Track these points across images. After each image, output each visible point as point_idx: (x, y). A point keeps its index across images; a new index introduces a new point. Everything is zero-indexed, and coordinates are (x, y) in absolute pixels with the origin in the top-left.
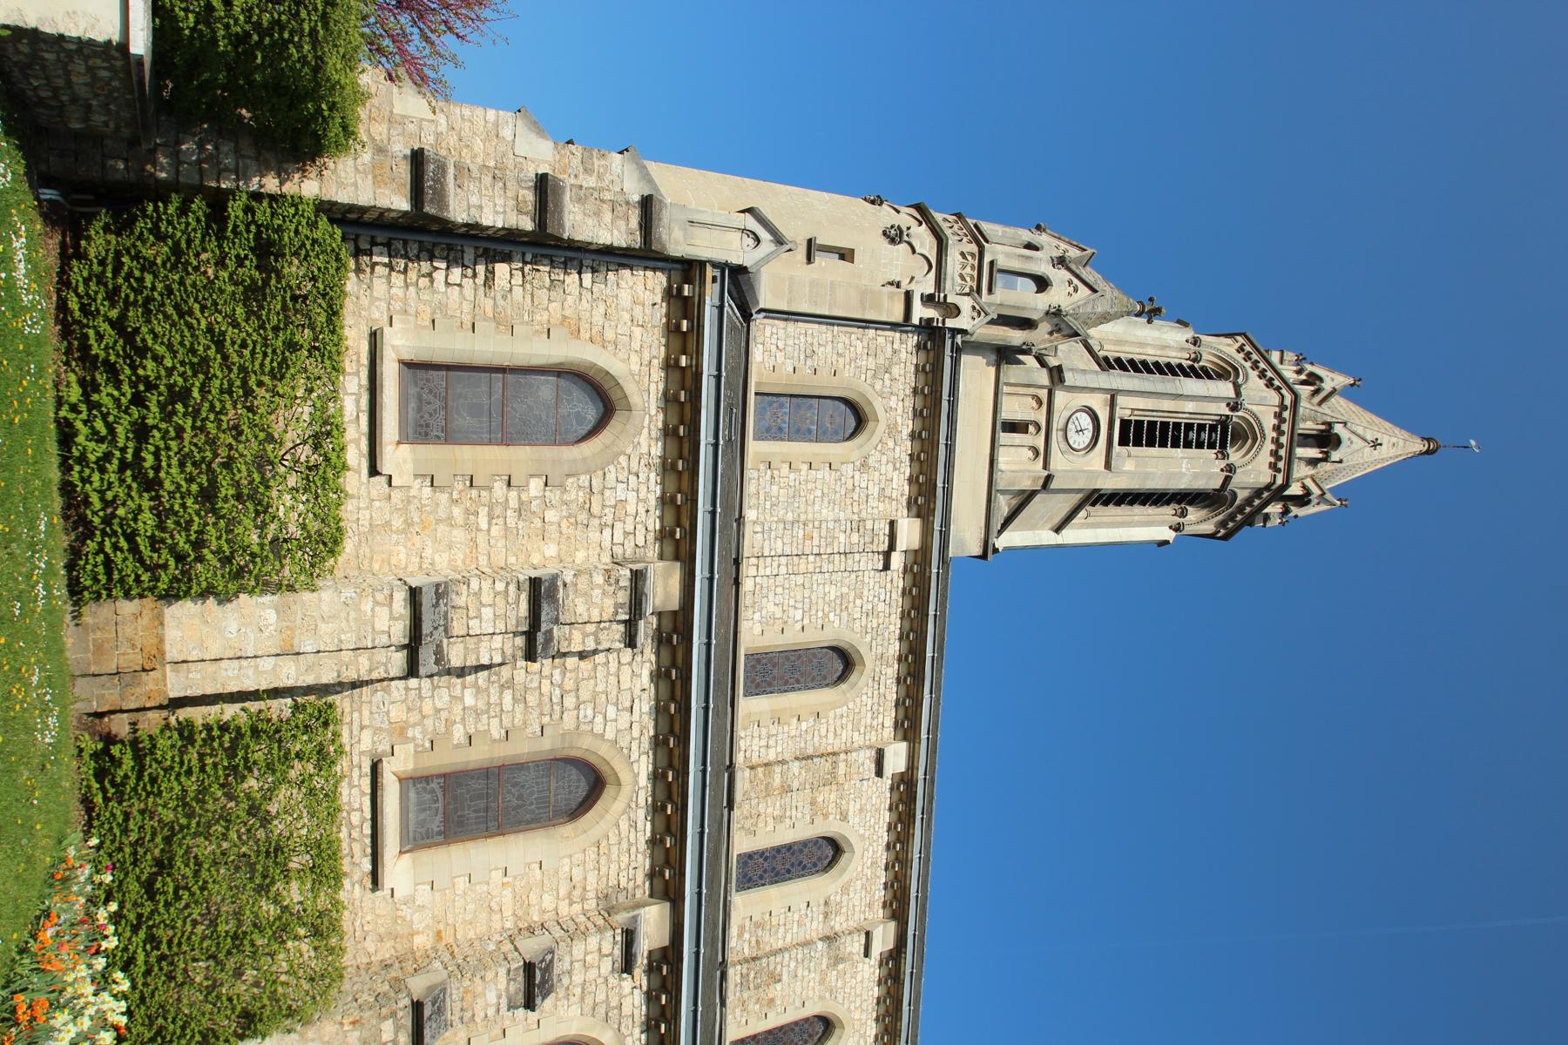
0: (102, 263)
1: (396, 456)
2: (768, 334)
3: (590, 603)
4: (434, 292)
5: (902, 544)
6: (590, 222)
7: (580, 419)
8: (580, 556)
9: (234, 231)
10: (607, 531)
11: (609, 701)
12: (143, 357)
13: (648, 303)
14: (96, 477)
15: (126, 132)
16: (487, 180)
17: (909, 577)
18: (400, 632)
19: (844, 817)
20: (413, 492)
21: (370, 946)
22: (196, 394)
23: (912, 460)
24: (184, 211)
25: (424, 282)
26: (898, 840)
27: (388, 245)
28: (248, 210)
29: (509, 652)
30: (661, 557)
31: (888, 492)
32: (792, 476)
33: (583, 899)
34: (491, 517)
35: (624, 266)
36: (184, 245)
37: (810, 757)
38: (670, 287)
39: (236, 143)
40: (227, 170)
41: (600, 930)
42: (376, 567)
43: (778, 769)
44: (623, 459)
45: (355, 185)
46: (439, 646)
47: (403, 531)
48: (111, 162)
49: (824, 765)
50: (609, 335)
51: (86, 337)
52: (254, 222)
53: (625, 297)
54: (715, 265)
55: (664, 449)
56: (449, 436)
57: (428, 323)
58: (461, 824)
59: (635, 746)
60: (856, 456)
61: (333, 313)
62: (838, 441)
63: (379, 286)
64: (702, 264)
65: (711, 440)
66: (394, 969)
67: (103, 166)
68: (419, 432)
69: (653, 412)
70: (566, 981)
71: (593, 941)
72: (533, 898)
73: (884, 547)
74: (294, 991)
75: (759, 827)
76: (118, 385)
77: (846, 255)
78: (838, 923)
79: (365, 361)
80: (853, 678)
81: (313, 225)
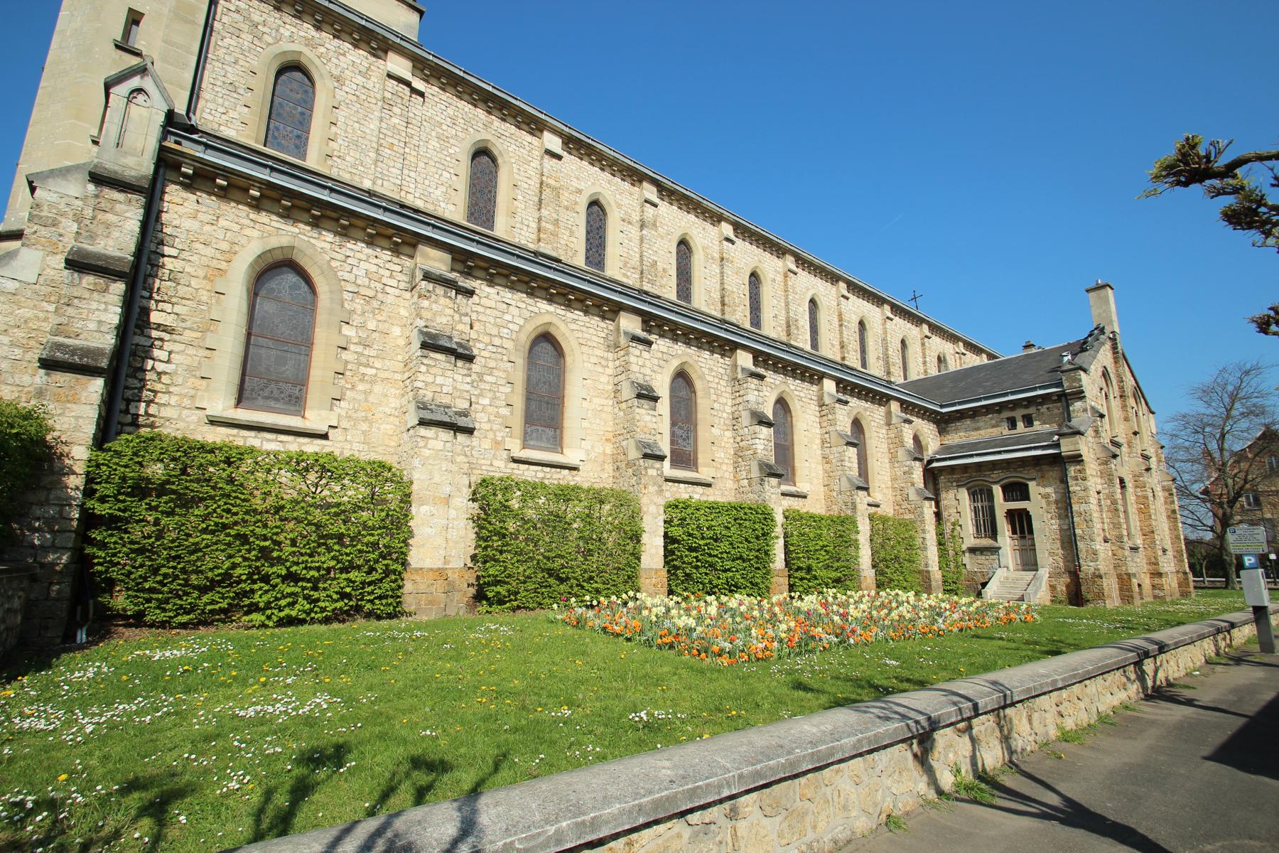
0: (148, 601)
1: (314, 419)
2: (211, 118)
3: (441, 313)
4: (176, 373)
5: (407, 75)
6: (116, 234)
7: (294, 287)
8: (403, 312)
9: (124, 511)
10: (388, 289)
11: (502, 317)
12: (231, 576)
13: (196, 206)
14: (321, 604)
15: (25, 584)
16: (70, 311)
17: (433, 80)
18: (445, 435)
19: (580, 191)
20: (343, 413)
21: (605, 476)
22: (267, 543)
23: (338, 38)
24: (103, 545)
25: (165, 379)
26: (600, 161)
27: (128, 401)
28: (103, 500)
29: (466, 372)
30: (412, 257)
31: (364, 70)
32: (340, 141)
33: (607, 360)
34: (367, 366)
35: (158, 218)
36: (136, 546)
37: (540, 201)
38: (181, 184)
39: (32, 504)
40: (61, 512)
41: (627, 354)
42: (393, 444)
43: (543, 224)
44: (334, 264)
45: (77, 418)
46: (456, 413)
47: (371, 423)
48: (53, 594)
49: (547, 193)
50: (225, 246)
51: (211, 611)
52: (115, 496)
53: (188, 224)
54: (164, 138)
55: (329, 231)
56: (301, 382)
57: (204, 382)
58: (553, 419)
59: (530, 308)
60: (331, 84)
61: (203, 448)
62: (314, 93)
63: (166, 412)
64: (162, 150)
65: (327, 192)
66: (620, 463)
67: (57, 600)
68: (296, 403)
69: (297, 230)
70: (647, 378)
71: (632, 359)
72: (601, 387)
73: (407, 90)
74: (624, 514)
75: (573, 249)
76: (253, 591)
77: (134, 18)
78: (635, 217)
79: (235, 431)
80: (496, 152)
81: (118, 454)
